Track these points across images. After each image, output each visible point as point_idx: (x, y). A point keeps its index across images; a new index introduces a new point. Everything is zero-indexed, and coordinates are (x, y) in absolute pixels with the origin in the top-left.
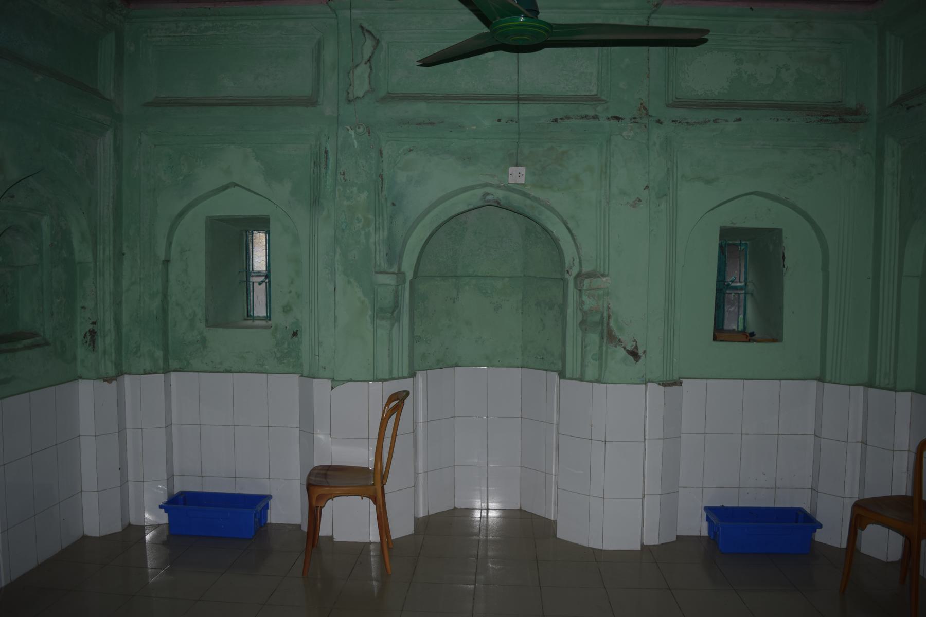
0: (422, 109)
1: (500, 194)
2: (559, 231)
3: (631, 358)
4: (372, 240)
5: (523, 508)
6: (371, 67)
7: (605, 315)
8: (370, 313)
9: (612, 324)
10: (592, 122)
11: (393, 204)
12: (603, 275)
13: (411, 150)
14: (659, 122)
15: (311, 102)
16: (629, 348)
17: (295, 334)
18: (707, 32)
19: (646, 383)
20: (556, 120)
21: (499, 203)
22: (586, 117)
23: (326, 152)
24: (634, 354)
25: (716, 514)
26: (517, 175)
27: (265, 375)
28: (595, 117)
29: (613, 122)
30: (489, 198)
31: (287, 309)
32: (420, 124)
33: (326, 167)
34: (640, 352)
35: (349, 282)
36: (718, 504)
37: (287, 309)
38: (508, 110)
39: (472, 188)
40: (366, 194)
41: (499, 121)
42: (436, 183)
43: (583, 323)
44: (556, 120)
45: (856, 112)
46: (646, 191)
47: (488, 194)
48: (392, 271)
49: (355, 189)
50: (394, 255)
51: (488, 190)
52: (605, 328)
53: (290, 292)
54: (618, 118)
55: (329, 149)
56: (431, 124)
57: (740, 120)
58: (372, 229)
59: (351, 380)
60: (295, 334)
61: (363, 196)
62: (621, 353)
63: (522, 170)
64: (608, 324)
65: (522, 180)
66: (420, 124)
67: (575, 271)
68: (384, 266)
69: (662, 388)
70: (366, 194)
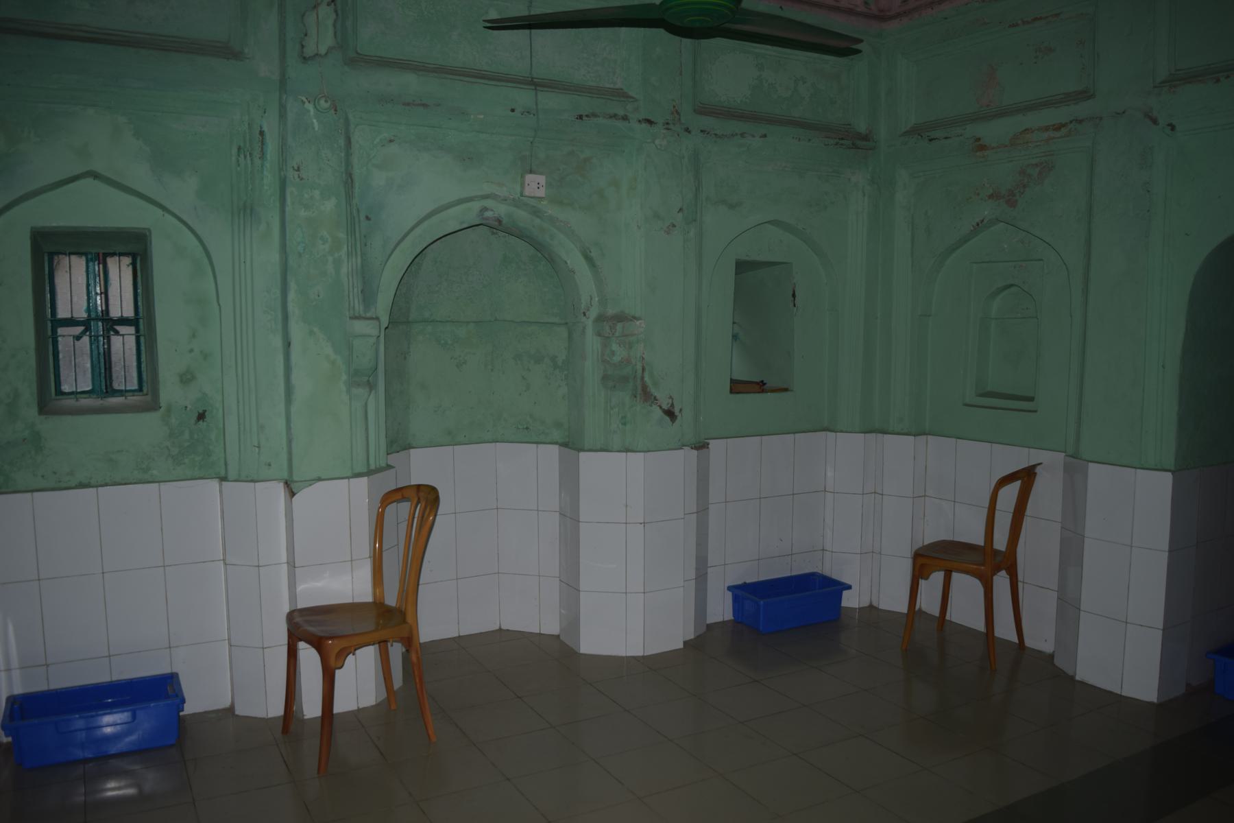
0: (411, 83)
1: (501, 210)
2: (575, 260)
3: (667, 419)
4: (344, 270)
5: (504, 627)
6: (336, 11)
7: (639, 367)
8: (344, 377)
9: (646, 379)
10: (620, 124)
11: (368, 218)
12: (635, 318)
13: (391, 141)
14: (687, 130)
15: (228, 52)
16: (665, 407)
17: (201, 417)
18: (860, 41)
19: (701, 446)
20: (580, 117)
21: (500, 222)
22: (615, 116)
23: (262, 133)
24: (670, 414)
25: (743, 593)
26: (536, 185)
27: (91, 491)
28: (625, 118)
29: (644, 125)
30: (488, 214)
31: (187, 378)
32: (408, 104)
33: (263, 156)
34: (676, 411)
35: (311, 333)
36: (740, 582)
37: (187, 378)
38: (523, 97)
39: (470, 199)
40: (333, 201)
41: (513, 110)
42: (422, 188)
43: (605, 378)
44: (580, 117)
45: (866, 138)
46: (680, 214)
47: (485, 209)
48: (368, 315)
49: (317, 193)
50: (368, 296)
51: (489, 203)
52: (86, 402)
53: (191, 351)
54: (650, 122)
55: (265, 129)
56: (425, 106)
57: (765, 136)
58: (343, 252)
59: (319, 479)
60: (201, 417)
61: (329, 205)
62: (657, 413)
63: (542, 179)
64: (643, 378)
65: (541, 193)
66: (408, 104)
67: (593, 313)
68: (359, 308)
69: (695, 452)
70: (333, 201)
